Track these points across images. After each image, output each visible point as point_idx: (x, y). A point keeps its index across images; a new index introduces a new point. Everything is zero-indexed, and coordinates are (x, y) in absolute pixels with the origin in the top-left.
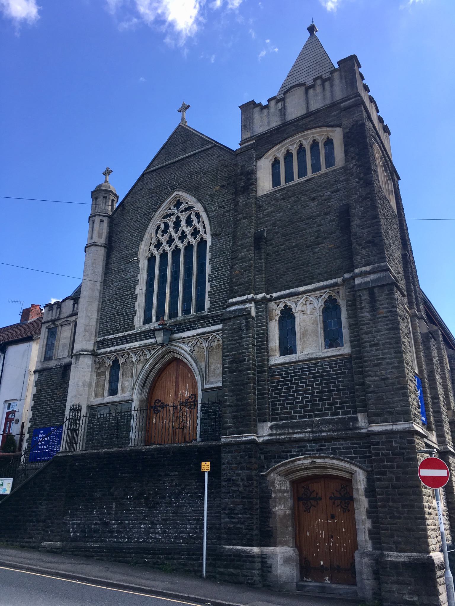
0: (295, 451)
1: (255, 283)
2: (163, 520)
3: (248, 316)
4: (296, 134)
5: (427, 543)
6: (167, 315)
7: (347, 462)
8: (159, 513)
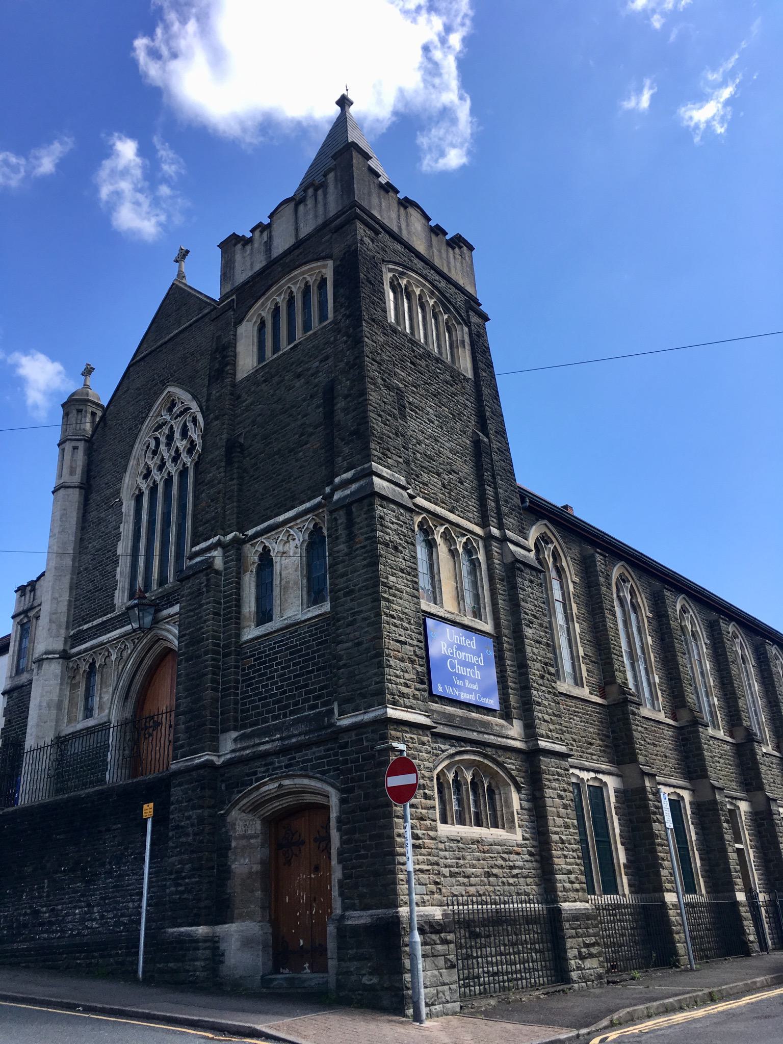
2: (101, 898)
5: (395, 893)
6: (156, 582)
7: (316, 778)
8: (97, 890)
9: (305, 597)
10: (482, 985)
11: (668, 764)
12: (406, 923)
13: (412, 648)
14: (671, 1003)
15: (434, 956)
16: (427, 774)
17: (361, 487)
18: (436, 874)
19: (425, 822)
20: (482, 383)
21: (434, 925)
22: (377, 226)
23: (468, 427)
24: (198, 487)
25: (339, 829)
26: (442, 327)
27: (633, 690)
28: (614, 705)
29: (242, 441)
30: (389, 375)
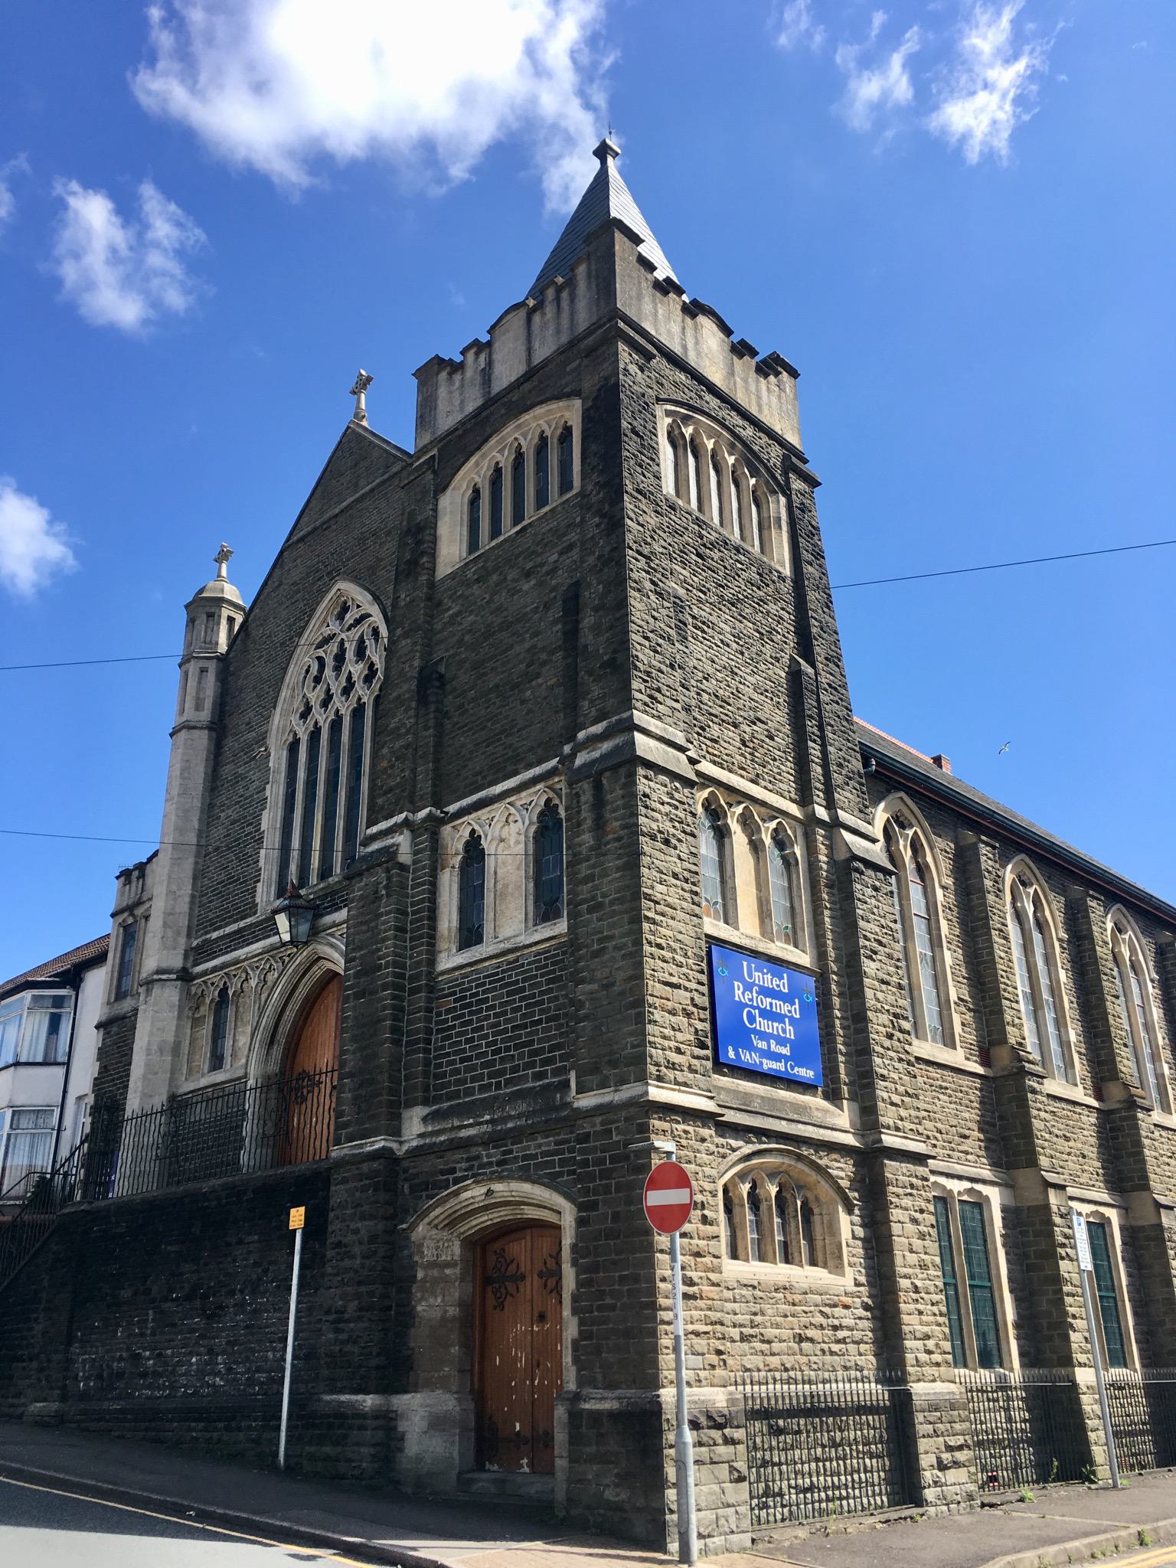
0: (461, 1170)
1: (414, 786)
2: (228, 1343)
3: (390, 865)
4: (505, 425)
5: (655, 1364)
6: (316, 872)
8: (222, 1330)
9: (531, 908)
10: (785, 1506)
11: (1086, 1168)
12: (671, 1413)
13: (688, 995)
14: (1077, 1549)
15: (713, 1463)
16: (708, 1186)
17: (617, 749)
18: (719, 1339)
19: (703, 1259)
20: (806, 583)
21: (715, 1416)
22: (650, 347)
23: (782, 651)
24: (377, 739)
25: (574, 1263)
26: (748, 498)
27: (1036, 1056)
28: (1003, 1077)
29: (442, 669)
30: (663, 575)
